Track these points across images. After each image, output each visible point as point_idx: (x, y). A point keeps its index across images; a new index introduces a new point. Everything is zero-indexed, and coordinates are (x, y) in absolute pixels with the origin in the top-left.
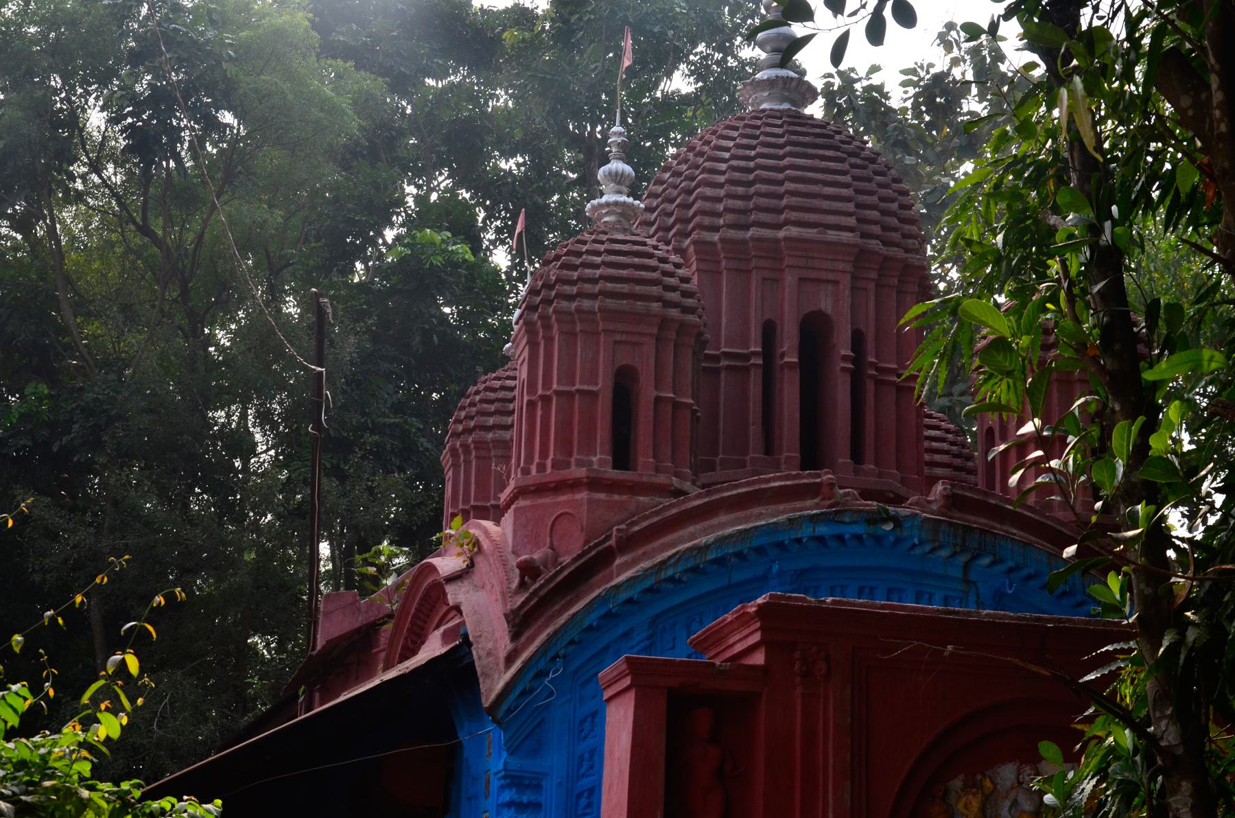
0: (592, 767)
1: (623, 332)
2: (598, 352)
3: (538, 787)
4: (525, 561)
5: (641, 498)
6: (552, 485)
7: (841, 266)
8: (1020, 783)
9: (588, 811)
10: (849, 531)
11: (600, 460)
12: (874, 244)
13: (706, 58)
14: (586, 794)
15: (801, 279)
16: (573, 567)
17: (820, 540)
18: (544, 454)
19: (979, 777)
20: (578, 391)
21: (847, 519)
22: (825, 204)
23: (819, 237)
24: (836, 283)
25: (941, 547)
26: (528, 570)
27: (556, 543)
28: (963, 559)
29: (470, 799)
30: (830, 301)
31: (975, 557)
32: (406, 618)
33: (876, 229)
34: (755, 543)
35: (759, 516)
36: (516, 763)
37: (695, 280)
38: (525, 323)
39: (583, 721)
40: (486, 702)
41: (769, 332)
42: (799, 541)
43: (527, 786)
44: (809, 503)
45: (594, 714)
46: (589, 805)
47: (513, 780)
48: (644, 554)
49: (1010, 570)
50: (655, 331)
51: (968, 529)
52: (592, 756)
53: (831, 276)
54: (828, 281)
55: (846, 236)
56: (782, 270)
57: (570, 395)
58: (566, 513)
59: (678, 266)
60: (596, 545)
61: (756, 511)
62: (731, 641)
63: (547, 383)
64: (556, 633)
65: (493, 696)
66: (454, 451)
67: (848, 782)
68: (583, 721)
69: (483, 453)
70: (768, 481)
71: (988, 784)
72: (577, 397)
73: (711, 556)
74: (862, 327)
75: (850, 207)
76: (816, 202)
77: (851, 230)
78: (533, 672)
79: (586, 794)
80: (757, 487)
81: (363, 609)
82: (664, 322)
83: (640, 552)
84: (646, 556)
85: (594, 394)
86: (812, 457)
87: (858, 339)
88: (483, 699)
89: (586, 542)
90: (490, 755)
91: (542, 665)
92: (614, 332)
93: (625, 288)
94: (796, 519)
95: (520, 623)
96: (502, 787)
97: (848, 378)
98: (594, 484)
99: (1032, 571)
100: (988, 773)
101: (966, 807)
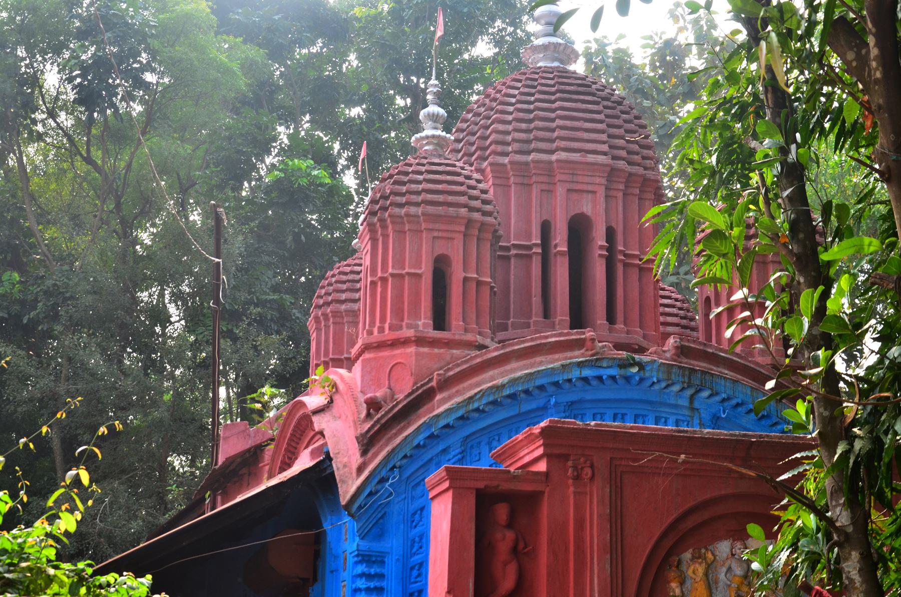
0: (421, 547)
1: (439, 230)
3: (383, 562)
5: (455, 351)
6: (390, 343)
7: (597, 180)
8: (733, 555)
9: (419, 579)
10: (606, 373)
11: (424, 323)
12: (621, 164)
14: (417, 568)
15: (568, 190)
16: (405, 402)
17: (585, 380)
18: (383, 319)
19: (703, 551)
20: (408, 274)
21: (605, 365)
22: (586, 135)
24: (594, 192)
25: (673, 384)
26: (373, 405)
27: (392, 385)
28: (689, 392)
30: (590, 206)
31: (698, 391)
34: (539, 382)
35: (541, 363)
36: (365, 545)
37: (491, 191)
39: (414, 514)
40: (344, 501)
41: (546, 229)
42: (570, 381)
43: (374, 562)
44: (577, 353)
45: (422, 509)
46: (419, 575)
47: (364, 558)
48: (457, 392)
49: (724, 400)
50: (463, 229)
51: (693, 371)
52: (421, 540)
53: (590, 188)
55: (601, 159)
57: (401, 276)
58: (396, 364)
59: (479, 181)
61: (538, 359)
62: (522, 454)
63: (385, 268)
65: (348, 497)
67: (608, 556)
68: (414, 514)
69: (338, 320)
70: (547, 337)
72: (407, 277)
73: (507, 392)
74: (613, 225)
75: (604, 137)
76: (579, 134)
77: (605, 154)
78: (378, 479)
79: (417, 568)
80: (538, 342)
81: (252, 435)
82: (469, 223)
83: (454, 390)
84: (458, 393)
85: (418, 276)
86: (578, 320)
87: (610, 234)
89: (415, 383)
90: (345, 539)
91: (383, 473)
92: (432, 230)
95: (367, 443)
96: (356, 563)
97: (604, 261)
98: (420, 341)
100: (710, 548)
101: (694, 572)
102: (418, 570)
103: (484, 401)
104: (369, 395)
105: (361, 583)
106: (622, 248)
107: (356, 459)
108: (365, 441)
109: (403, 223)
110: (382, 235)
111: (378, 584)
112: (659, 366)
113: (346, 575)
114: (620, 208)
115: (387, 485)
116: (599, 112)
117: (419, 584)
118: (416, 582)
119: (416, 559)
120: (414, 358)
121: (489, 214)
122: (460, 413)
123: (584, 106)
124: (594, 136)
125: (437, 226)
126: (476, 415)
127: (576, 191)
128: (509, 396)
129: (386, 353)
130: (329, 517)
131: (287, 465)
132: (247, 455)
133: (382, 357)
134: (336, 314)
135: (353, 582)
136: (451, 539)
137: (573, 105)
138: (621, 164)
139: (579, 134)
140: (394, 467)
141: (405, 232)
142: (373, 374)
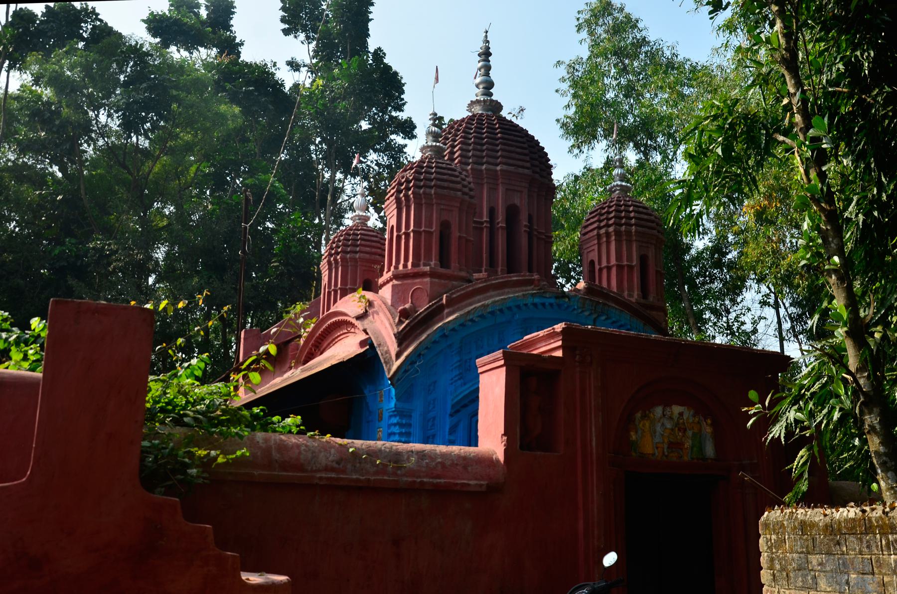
3: (410, 416)
8: (664, 415)
10: (547, 301)
12: (537, 176)
13: (375, 114)
17: (535, 305)
22: (517, 156)
24: (521, 192)
26: (404, 314)
28: (594, 316)
29: (368, 422)
31: (598, 316)
33: (538, 170)
35: (508, 293)
38: (396, 198)
41: (492, 212)
42: (526, 305)
44: (529, 288)
45: (435, 382)
46: (433, 425)
47: (398, 412)
51: (598, 302)
54: (518, 191)
55: (526, 171)
56: (498, 185)
61: (506, 290)
64: (420, 343)
65: (392, 373)
66: (329, 262)
73: (489, 310)
75: (528, 158)
76: (513, 155)
77: (528, 168)
85: (431, 233)
86: (511, 268)
87: (530, 218)
93: (446, 184)
95: (403, 339)
96: (390, 416)
98: (432, 274)
99: (623, 323)
105: (396, 430)
107: (393, 347)
113: (384, 423)
116: (524, 143)
121: (472, 197)
122: (462, 321)
128: (490, 313)
129: (409, 281)
131: (310, 357)
134: (355, 260)
137: (512, 137)
138: (537, 176)
139: (513, 155)
140: (420, 355)
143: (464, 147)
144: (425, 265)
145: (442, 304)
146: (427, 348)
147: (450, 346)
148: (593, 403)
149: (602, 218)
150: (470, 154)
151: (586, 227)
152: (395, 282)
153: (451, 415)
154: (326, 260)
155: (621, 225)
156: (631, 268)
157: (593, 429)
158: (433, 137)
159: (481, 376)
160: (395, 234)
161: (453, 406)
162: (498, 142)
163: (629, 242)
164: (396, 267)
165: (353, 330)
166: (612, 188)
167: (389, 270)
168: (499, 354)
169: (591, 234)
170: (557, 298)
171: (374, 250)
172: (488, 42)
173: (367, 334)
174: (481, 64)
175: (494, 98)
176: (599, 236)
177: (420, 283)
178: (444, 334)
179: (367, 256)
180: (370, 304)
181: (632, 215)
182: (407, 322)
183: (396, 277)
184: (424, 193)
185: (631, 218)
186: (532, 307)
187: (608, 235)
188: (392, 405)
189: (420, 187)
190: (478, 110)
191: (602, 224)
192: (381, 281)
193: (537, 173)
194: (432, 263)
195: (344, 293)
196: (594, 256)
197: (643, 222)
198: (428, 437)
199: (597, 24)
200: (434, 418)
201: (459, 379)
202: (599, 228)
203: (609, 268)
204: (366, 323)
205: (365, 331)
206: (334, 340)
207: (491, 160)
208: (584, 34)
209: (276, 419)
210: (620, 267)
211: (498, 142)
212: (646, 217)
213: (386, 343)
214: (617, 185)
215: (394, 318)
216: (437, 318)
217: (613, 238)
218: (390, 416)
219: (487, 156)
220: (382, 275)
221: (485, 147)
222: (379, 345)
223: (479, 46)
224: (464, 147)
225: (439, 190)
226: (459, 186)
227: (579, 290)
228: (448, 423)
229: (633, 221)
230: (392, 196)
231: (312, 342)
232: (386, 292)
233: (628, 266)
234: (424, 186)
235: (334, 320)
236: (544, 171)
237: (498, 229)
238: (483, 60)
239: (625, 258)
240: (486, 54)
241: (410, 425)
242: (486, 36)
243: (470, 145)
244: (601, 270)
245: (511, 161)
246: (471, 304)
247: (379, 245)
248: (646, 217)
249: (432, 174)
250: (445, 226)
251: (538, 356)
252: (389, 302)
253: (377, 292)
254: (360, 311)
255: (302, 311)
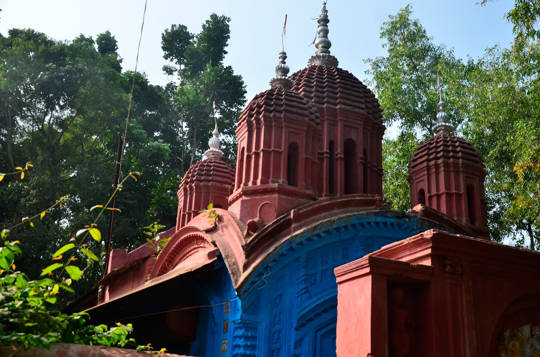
0: (280, 320)
1: (292, 128)
2: (282, 136)
4: (250, 222)
6: (261, 191)
7: (359, 122)
8: (532, 335)
9: (278, 341)
10: (390, 221)
14: (277, 333)
15: (345, 126)
16: (273, 227)
17: (377, 224)
19: (515, 331)
21: (389, 215)
22: (354, 98)
23: (352, 110)
24: (357, 129)
26: (253, 227)
27: (262, 216)
29: (214, 333)
32: (166, 254)
35: (352, 211)
39: (276, 298)
41: (332, 144)
42: (369, 223)
43: (250, 328)
44: (371, 208)
45: (281, 295)
46: (278, 338)
47: (244, 324)
48: (305, 223)
50: (306, 129)
53: (356, 126)
54: (354, 128)
55: (361, 111)
56: (337, 122)
58: (268, 203)
60: (283, 218)
61: (350, 209)
64: (268, 255)
65: (239, 283)
66: (185, 189)
67: (474, 332)
70: (354, 197)
71: (520, 335)
72: (272, 153)
73: (335, 226)
76: (351, 97)
77: (363, 109)
79: (277, 333)
80: (351, 199)
83: (303, 222)
85: (280, 153)
87: (365, 152)
88: (234, 284)
92: (289, 127)
93: (294, 110)
94: (369, 213)
95: (250, 251)
96: (236, 328)
97: (362, 166)
98: (280, 191)
100: (519, 329)
102: (278, 335)
103: (322, 230)
104: (249, 221)
105: (241, 342)
106: (369, 160)
107: (241, 259)
108: (248, 249)
109: (271, 122)
110: (256, 128)
111: (253, 343)
112: (418, 220)
114: (369, 140)
115: (263, 277)
117: (278, 344)
118: (276, 343)
119: (278, 327)
120: (277, 201)
122: (309, 236)
123: (352, 84)
124: (358, 99)
125: (292, 125)
126: (316, 238)
127: (348, 126)
128: (335, 229)
129: (258, 197)
130: (214, 298)
131: (164, 271)
132: (136, 263)
133: (255, 199)
134: (208, 187)
135: (234, 341)
136: (372, 310)
137: (349, 83)
139: (351, 97)
140: (267, 267)
141: (282, 128)
142: (249, 209)
143: (307, 89)
144: (273, 182)
145: (290, 219)
146: (274, 261)
147: (297, 260)
148: (466, 320)
149: (430, 152)
150: (313, 95)
151: (414, 161)
152: (244, 198)
153: (297, 329)
154: (182, 188)
155: (449, 158)
156: (459, 195)
157: (468, 350)
158: (282, 72)
159: (339, 286)
160: (246, 154)
161: (299, 320)
162: (337, 86)
163: (457, 173)
164: (246, 184)
165: (202, 245)
166: (437, 128)
167: (239, 187)
168: (365, 259)
169: (421, 166)
170: (397, 217)
171: (224, 180)
172: (326, 11)
173: (216, 246)
174: (320, 28)
175: (331, 54)
176: (428, 168)
177: (268, 199)
178: (291, 248)
179: (219, 184)
180: (220, 219)
181: (459, 149)
182: (255, 234)
183: (245, 193)
184: (274, 116)
185: (458, 152)
186: (374, 226)
187: (437, 166)
188: (238, 316)
189: (271, 112)
190: (317, 63)
191: (431, 157)
192: (230, 198)
193: (371, 114)
194: (281, 181)
195: (196, 214)
196: (424, 185)
197: (468, 156)
198: (273, 351)
199: (396, 34)
200: (280, 331)
201: (305, 293)
202: (428, 160)
203: (438, 196)
204: (215, 237)
205: (214, 243)
206: (185, 255)
207: (331, 100)
208: (385, 40)
209: (99, 328)
210: (449, 195)
211: (337, 86)
212: (470, 152)
213: (234, 255)
214: (442, 126)
215: (242, 231)
216: (285, 231)
217: (442, 169)
218: (236, 328)
219: (328, 96)
220: (232, 193)
221: (326, 89)
222: (227, 257)
223: (319, 14)
224: (307, 89)
225: (288, 115)
226: (306, 112)
227: (417, 212)
228: (294, 337)
229: (460, 155)
230: (243, 121)
231: (166, 257)
232: (236, 209)
233: (456, 194)
234: (275, 110)
235: (186, 236)
236: (376, 113)
237: (337, 159)
238: (323, 25)
239: (453, 187)
240: (324, 21)
241: (255, 338)
242: (325, 7)
243: (312, 87)
244: (430, 198)
245: (349, 102)
246: (317, 220)
247: (229, 175)
248: (470, 152)
249: (282, 100)
250: (293, 148)
251: (407, 264)
252: (238, 217)
253: (226, 209)
254: (210, 226)
255: (160, 231)
